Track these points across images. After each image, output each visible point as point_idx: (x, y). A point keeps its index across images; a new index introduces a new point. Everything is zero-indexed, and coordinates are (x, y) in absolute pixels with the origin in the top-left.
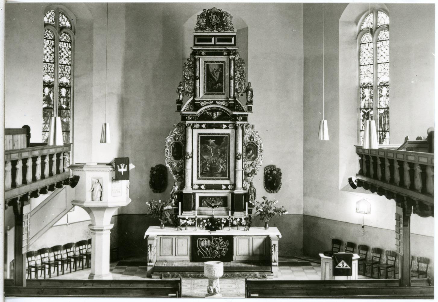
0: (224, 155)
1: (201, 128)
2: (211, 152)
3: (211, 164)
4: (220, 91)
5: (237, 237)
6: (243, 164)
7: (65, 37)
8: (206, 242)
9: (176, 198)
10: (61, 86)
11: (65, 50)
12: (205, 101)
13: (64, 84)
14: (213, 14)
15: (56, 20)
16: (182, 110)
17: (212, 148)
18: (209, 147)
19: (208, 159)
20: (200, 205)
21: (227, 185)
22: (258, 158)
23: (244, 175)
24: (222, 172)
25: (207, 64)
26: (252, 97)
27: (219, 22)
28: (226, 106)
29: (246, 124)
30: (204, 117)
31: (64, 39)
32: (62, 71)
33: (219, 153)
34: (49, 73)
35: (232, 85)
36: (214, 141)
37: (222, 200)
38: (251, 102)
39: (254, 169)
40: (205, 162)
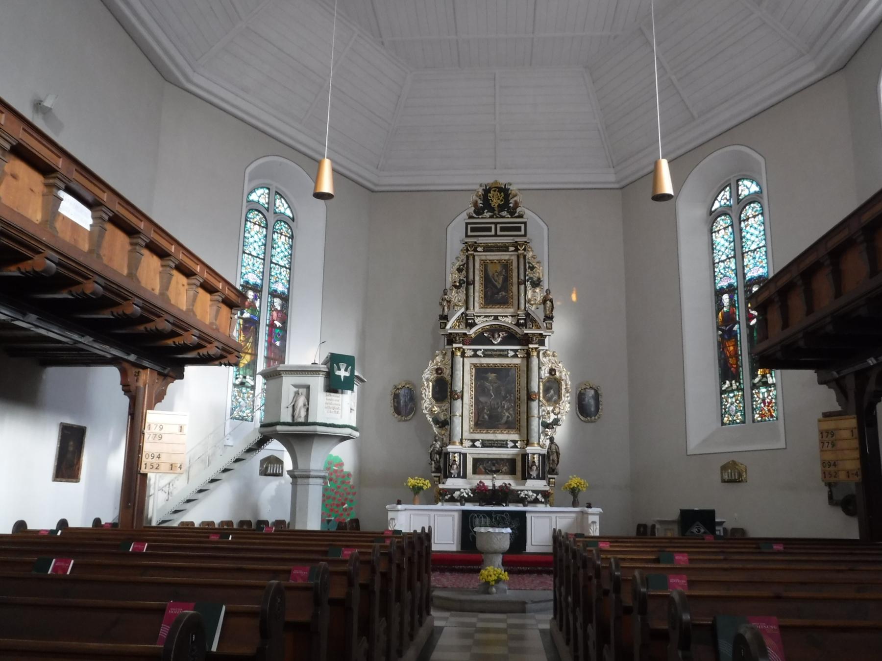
0: (511, 396)
1: (475, 355)
2: (491, 391)
3: (492, 409)
4: (504, 302)
5: (533, 515)
6: (540, 410)
7: (258, 218)
8: (483, 520)
9: (436, 459)
10: (274, 294)
11: (283, 246)
12: (482, 317)
13: (279, 292)
14: (493, 191)
15: (271, 203)
16: (448, 327)
17: (492, 386)
18: (487, 384)
19: (486, 403)
20: (475, 472)
21: (515, 442)
22: (562, 401)
23: (541, 427)
24: (507, 422)
25: (485, 264)
26: (552, 310)
27: (502, 202)
28: (513, 323)
29: (543, 351)
30: (480, 339)
31: (255, 220)
32: (276, 274)
33: (503, 393)
34: (256, 272)
35: (522, 293)
36: (495, 376)
37: (507, 464)
38: (551, 318)
39: (556, 417)
40: (481, 406)
